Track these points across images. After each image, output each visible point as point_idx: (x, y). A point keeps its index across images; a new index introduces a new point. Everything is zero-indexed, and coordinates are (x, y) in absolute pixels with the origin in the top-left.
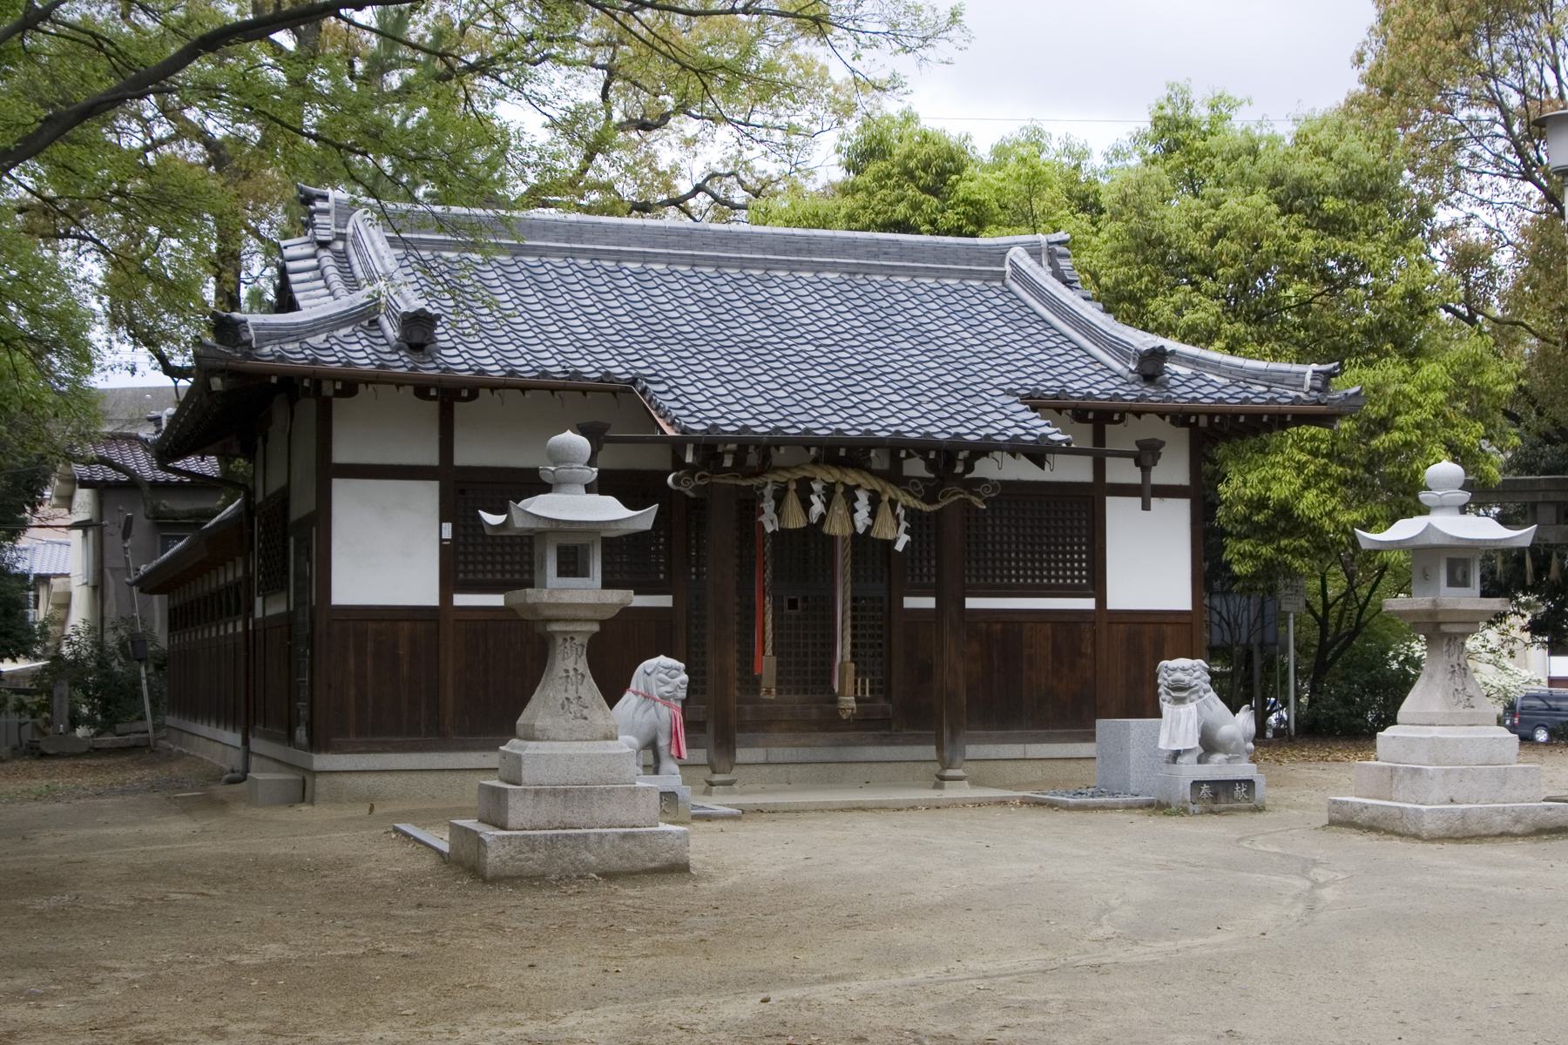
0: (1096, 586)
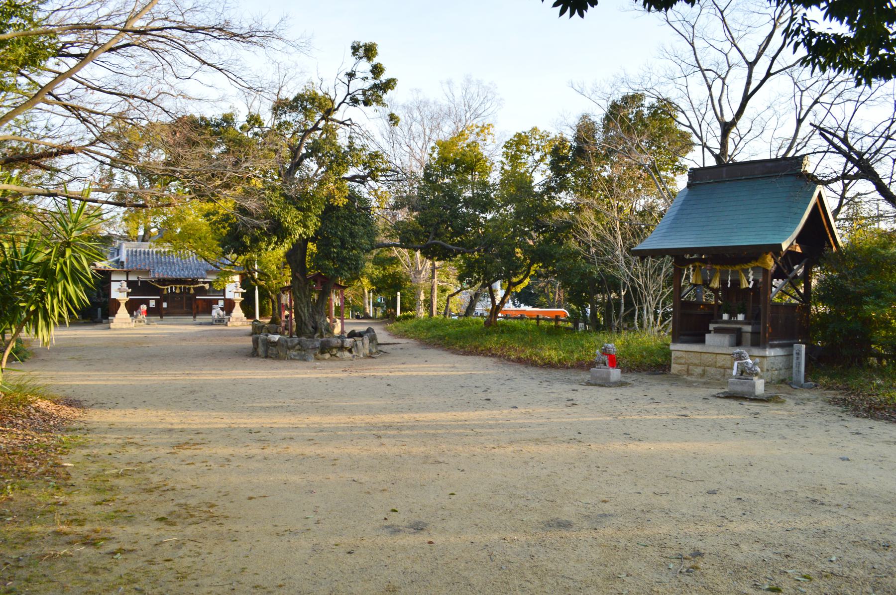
0: (224, 295)
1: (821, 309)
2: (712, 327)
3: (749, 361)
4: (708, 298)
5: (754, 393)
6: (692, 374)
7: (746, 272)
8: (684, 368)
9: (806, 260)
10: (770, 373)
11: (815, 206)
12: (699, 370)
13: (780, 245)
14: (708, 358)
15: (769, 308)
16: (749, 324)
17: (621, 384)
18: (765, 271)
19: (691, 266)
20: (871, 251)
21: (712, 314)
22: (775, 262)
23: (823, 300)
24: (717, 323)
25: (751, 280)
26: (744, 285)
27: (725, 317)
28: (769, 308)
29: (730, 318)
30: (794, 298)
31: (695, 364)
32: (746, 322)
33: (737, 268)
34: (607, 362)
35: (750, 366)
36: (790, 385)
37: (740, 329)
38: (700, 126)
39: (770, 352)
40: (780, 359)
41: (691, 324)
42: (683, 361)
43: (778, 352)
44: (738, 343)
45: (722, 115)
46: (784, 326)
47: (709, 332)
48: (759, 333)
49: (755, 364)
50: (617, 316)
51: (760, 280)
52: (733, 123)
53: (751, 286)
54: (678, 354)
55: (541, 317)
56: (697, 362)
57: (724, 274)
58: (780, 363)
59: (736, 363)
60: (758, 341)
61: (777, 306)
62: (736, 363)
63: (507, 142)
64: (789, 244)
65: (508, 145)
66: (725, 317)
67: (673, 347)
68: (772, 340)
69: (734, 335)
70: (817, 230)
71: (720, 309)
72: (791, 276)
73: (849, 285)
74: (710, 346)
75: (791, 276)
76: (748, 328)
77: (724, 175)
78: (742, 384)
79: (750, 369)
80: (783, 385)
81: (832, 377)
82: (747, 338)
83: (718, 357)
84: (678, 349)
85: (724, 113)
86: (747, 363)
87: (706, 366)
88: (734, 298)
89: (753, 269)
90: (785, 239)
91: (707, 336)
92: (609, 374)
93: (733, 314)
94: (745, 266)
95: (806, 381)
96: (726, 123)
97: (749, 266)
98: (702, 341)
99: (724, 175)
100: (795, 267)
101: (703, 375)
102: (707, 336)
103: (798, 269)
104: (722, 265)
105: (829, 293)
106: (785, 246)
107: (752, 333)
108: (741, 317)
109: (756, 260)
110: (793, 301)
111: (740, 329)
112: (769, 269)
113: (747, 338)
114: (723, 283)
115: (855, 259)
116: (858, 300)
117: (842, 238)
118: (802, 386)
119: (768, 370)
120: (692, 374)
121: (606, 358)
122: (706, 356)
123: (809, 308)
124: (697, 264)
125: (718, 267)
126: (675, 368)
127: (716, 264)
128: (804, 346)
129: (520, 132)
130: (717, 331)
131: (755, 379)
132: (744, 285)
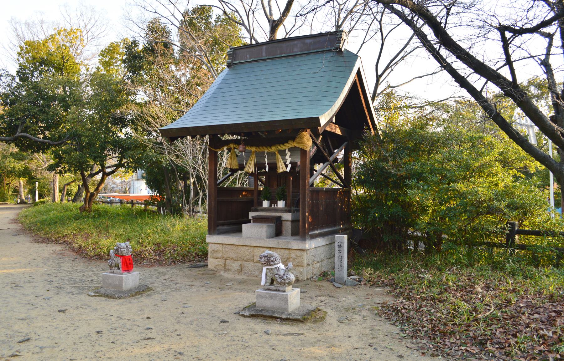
1: (361, 191)
2: (251, 215)
3: (282, 266)
4: (241, 182)
5: (286, 309)
6: (229, 270)
7: (283, 153)
8: (221, 262)
9: (346, 143)
10: (311, 267)
11: (354, 85)
12: (236, 265)
13: (318, 119)
14: (246, 252)
15: (308, 193)
16: (289, 211)
17: (141, 291)
18: (303, 152)
19: (225, 148)
20: (410, 134)
21: (252, 202)
22: (314, 143)
23: (361, 183)
24: (256, 210)
25: (288, 163)
26: (281, 168)
27: (266, 204)
28: (308, 193)
29: (271, 205)
30: (335, 182)
31: (232, 259)
32: (287, 210)
33: (274, 149)
34: (120, 265)
35: (282, 273)
36: (333, 281)
37: (280, 217)
38: (248, 16)
39: (311, 244)
40: (321, 249)
41: (230, 213)
42: (220, 255)
43: (320, 242)
44: (278, 233)
45: (271, 14)
46: (327, 213)
47: (249, 221)
48: (298, 221)
49: (287, 270)
50: (188, 203)
51: (299, 163)
52: (280, 21)
53: (288, 170)
54: (215, 247)
55: (135, 202)
56: (234, 256)
57: (260, 156)
58: (322, 254)
59: (264, 269)
60: (299, 232)
61: (317, 192)
62: (264, 269)
63: (102, 51)
64: (328, 119)
65: (103, 54)
66: (266, 204)
67: (210, 239)
68: (313, 230)
69: (273, 225)
70: (355, 110)
71: (261, 196)
72: (331, 159)
73: (389, 166)
74: (247, 238)
75: (331, 159)
76: (288, 217)
77: (264, 54)
78: (271, 297)
79: (281, 277)
80: (325, 284)
81: (375, 267)
82: (287, 227)
83: (256, 250)
84: (214, 241)
85: (273, 12)
86: (278, 269)
87: (243, 260)
88: (288, 186)
89: (290, 150)
90: (323, 113)
91: (245, 227)
92: (121, 280)
93: (273, 201)
94: (282, 147)
95: (349, 275)
96: (274, 21)
97: (286, 147)
98: (240, 231)
99: (264, 54)
100: (336, 151)
101: (240, 270)
102: (245, 227)
103: (338, 153)
104: (257, 146)
105: (373, 176)
106: (323, 121)
107: (292, 221)
108: (281, 204)
109: (293, 139)
110: (336, 186)
111: (280, 217)
112: (308, 149)
113: (287, 227)
114: (260, 166)
115: (393, 141)
116: (400, 183)
117: (380, 121)
118: (345, 284)
119: (308, 265)
120: (229, 270)
121: (119, 260)
122: (244, 249)
123: (350, 192)
124: (232, 146)
125: (253, 149)
126: (212, 263)
127: (252, 146)
128: (346, 237)
129: (113, 41)
130: (257, 220)
131: (289, 289)
132: (281, 168)
